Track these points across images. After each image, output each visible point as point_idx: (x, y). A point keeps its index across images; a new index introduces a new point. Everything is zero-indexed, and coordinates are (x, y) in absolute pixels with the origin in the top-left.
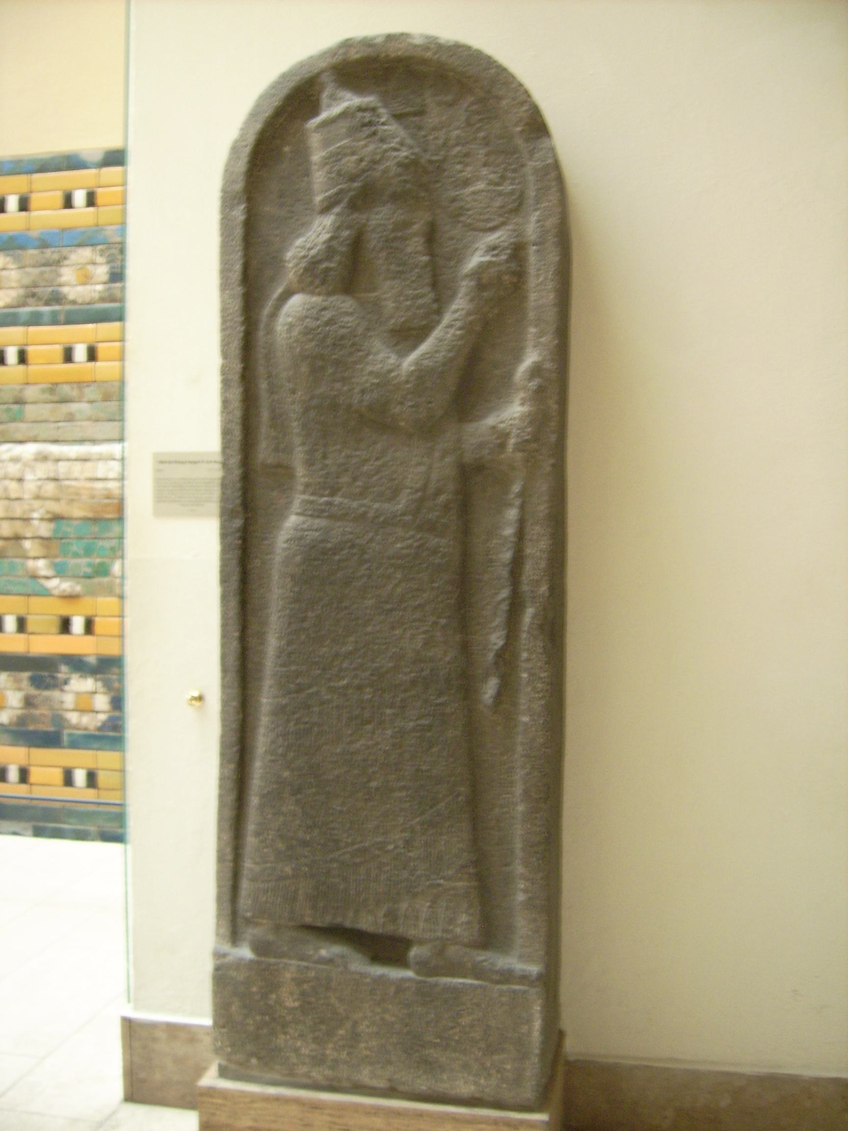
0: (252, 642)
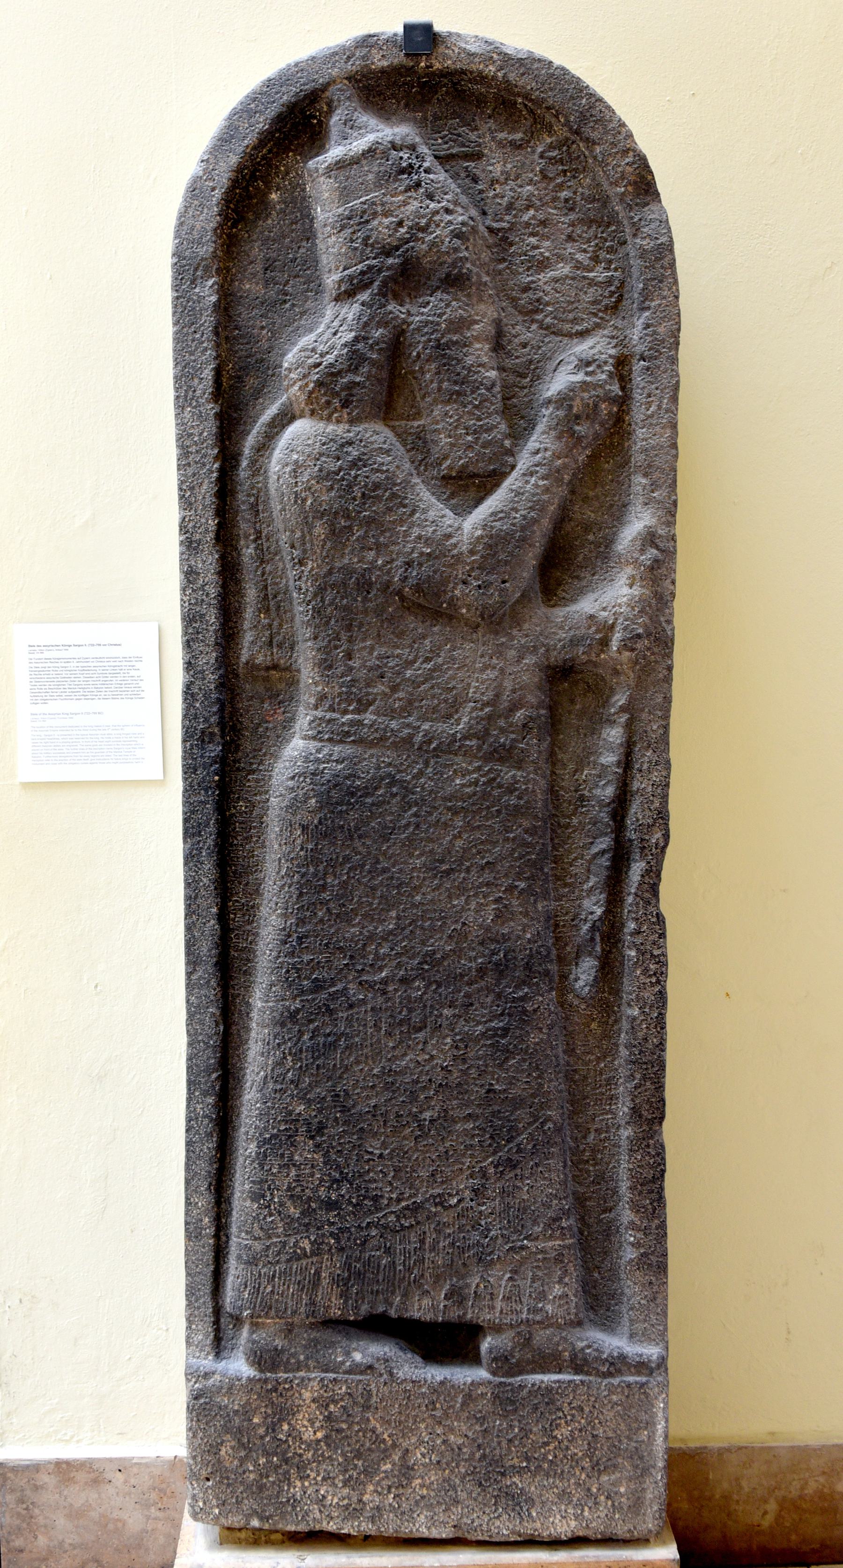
0: (237, 919)
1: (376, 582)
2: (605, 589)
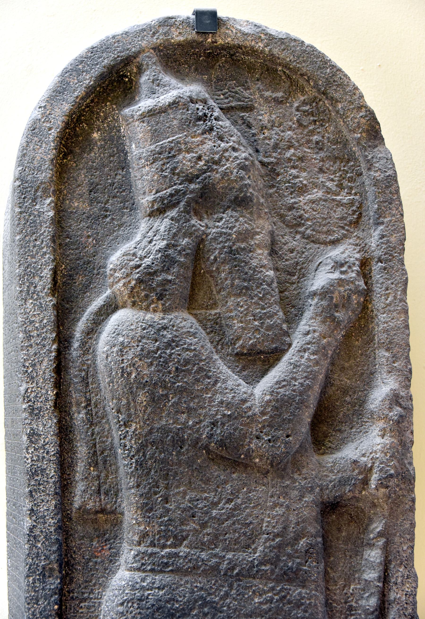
1: (188, 439)
2: (362, 439)
